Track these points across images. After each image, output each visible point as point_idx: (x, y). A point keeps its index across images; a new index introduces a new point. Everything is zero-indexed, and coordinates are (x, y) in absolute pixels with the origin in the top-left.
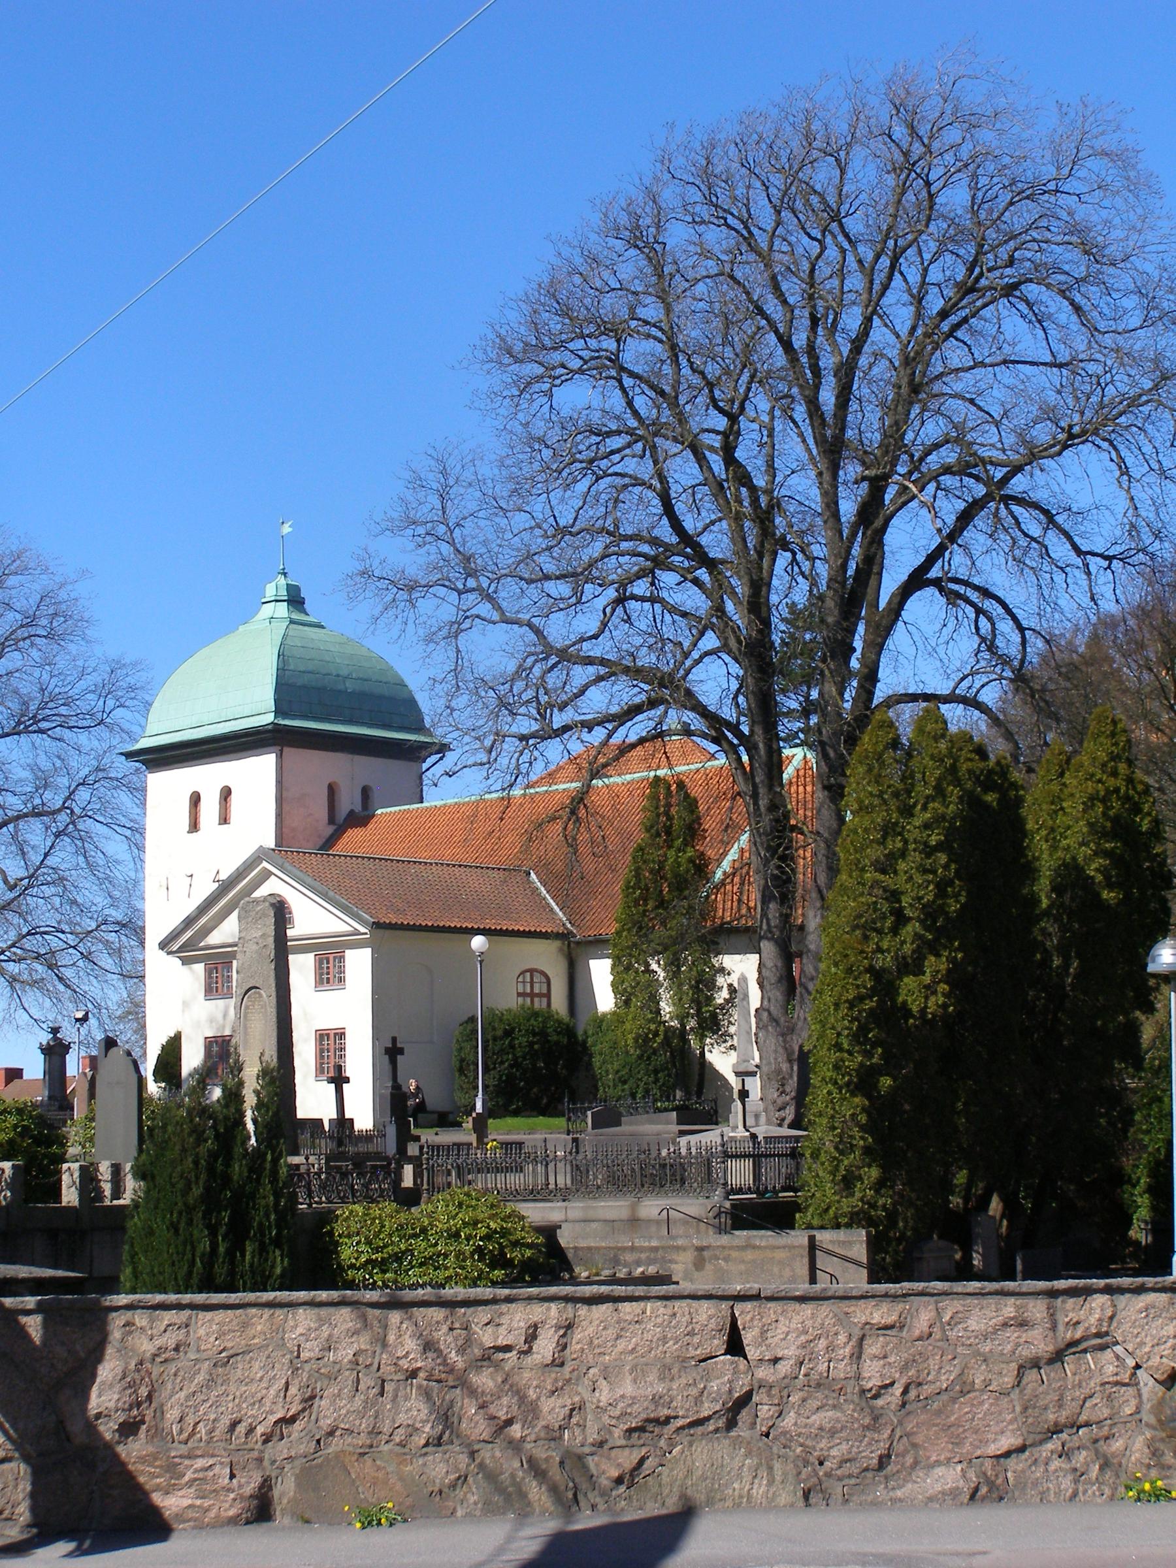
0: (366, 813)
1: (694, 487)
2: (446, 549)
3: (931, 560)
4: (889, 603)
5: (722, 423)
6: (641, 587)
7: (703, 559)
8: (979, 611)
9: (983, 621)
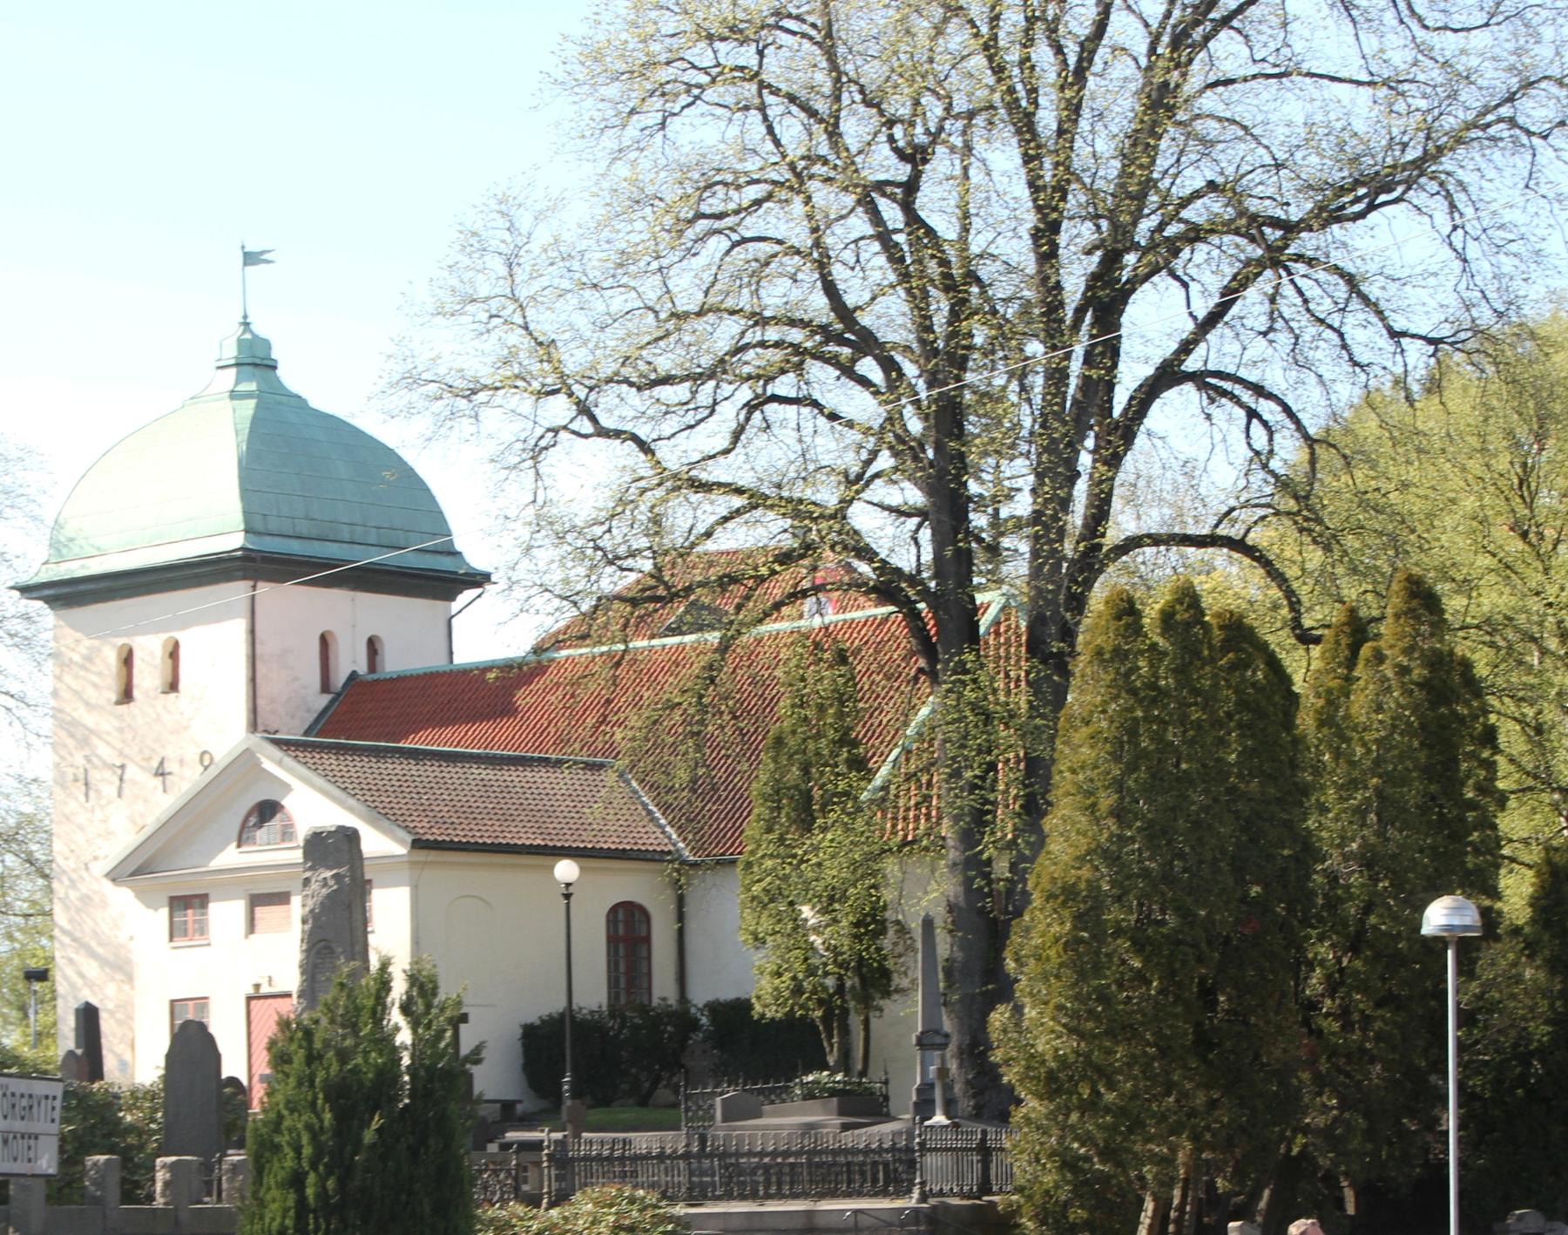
0: (375, 676)
1: (856, 241)
2: (516, 337)
3: (1186, 348)
4: (1126, 410)
5: (902, 172)
6: (785, 385)
7: (867, 343)
8: (1252, 414)
9: (1257, 429)
